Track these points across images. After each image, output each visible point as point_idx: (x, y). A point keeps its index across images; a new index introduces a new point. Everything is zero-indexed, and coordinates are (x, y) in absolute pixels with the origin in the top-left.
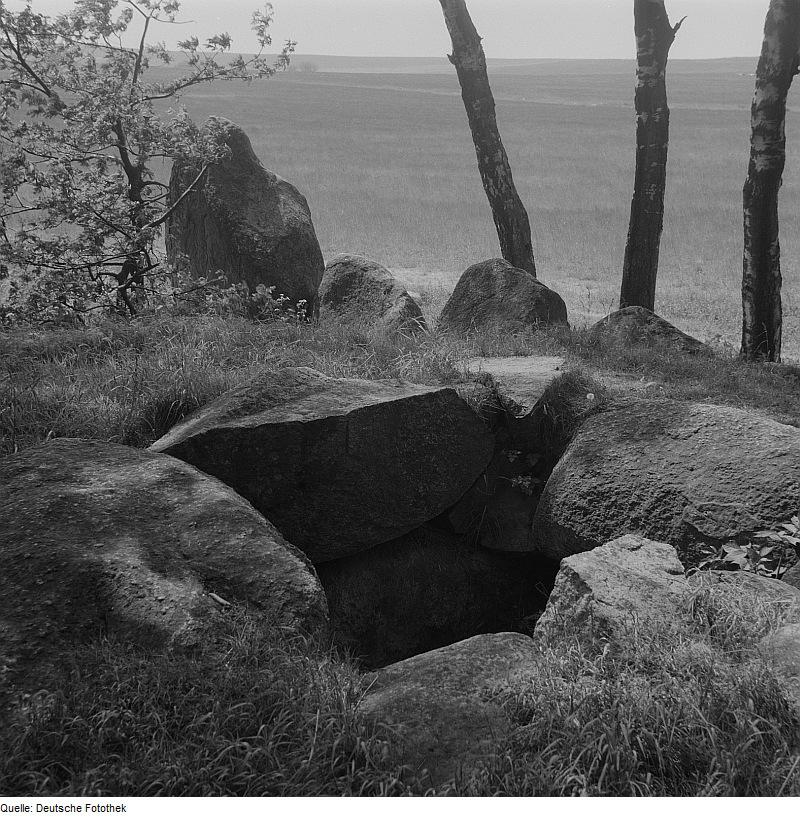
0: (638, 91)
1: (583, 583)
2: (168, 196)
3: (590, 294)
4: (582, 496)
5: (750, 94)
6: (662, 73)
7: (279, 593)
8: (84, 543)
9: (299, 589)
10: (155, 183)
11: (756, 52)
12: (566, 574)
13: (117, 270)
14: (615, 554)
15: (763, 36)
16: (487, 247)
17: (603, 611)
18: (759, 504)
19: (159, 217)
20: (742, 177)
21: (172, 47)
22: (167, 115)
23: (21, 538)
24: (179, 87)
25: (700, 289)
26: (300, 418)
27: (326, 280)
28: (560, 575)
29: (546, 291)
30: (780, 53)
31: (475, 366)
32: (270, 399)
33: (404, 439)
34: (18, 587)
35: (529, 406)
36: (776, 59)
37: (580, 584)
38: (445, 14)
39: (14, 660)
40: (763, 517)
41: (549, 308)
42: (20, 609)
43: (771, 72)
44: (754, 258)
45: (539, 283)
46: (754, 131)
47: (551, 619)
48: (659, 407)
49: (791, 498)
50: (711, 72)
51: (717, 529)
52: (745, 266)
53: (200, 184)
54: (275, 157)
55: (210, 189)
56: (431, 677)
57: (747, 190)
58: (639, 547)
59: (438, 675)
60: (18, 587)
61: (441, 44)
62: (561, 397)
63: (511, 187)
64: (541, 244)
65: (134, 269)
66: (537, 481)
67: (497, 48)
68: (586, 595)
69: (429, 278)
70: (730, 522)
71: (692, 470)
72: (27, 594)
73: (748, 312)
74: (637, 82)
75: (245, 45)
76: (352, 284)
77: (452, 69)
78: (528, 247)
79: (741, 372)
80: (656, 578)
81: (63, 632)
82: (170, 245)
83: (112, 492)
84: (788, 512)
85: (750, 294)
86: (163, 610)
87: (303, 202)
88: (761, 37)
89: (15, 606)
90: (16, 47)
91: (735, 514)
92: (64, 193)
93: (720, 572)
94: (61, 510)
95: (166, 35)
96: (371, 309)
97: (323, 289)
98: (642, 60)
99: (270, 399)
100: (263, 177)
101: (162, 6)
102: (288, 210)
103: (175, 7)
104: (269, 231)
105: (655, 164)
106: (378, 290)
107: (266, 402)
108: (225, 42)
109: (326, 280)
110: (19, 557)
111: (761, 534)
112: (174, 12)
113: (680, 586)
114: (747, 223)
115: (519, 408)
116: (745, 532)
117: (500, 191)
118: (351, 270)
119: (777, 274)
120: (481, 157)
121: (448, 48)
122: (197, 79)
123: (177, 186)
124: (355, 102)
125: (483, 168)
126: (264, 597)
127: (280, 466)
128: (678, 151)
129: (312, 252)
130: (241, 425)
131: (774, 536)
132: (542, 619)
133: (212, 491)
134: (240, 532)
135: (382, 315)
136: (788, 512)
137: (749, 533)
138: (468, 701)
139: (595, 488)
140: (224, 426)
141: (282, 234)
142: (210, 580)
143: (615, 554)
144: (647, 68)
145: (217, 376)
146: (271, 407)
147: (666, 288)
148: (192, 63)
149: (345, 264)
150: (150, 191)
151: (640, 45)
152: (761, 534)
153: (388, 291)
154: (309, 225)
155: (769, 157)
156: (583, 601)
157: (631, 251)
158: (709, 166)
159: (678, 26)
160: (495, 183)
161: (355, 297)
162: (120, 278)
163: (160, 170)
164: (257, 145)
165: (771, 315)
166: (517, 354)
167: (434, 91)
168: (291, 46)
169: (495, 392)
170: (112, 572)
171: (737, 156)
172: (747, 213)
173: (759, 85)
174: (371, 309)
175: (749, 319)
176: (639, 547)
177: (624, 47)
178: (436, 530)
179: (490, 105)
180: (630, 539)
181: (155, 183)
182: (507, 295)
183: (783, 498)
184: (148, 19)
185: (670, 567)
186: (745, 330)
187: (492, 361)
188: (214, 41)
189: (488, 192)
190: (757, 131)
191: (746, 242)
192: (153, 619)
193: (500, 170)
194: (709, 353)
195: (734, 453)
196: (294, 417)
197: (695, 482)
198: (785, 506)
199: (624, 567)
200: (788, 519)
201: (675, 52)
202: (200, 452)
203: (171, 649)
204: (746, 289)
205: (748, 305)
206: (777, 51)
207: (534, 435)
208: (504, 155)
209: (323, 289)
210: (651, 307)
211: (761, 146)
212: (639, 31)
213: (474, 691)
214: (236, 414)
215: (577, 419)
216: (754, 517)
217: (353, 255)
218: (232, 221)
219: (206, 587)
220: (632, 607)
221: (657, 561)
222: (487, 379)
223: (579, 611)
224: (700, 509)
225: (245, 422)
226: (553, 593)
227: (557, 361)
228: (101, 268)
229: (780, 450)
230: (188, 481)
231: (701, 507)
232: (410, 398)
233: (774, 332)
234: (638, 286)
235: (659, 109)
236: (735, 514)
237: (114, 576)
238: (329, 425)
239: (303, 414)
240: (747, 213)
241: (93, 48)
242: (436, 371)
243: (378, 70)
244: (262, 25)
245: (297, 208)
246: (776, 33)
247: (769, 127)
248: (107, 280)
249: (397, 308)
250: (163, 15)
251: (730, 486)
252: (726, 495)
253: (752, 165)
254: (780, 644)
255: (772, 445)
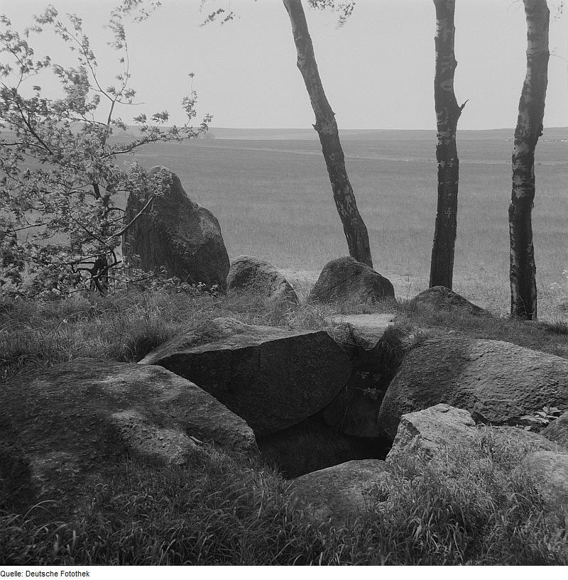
0: (438, 147)
1: (415, 428)
2: (124, 218)
3: (408, 277)
4: (409, 399)
5: (511, 149)
6: (453, 136)
7: (232, 437)
8: (111, 409)
9: (243, 434)
10: (117, 209)
11: (513, 124)
12: (404, 424)
13: (91, 266)
14: (433, 414)
15: (518, 112)
16: (340, 250)
17: (426, 444)
18: (522, 400)
19: (120, 231)
20: (509, 201)
21: (129, 122)
22: (125, 165)
23: (73, 406)
24: (135, 146)
25: (482, 277)
26: (230, 347)
27: (232, 273)
28: (401, 425)
29: (380, 278)
30: (530, 123)
31: (338, 320)
32: (209, 336)
33: (295, 363)
34: (75, 433)
35: (375, 341)
36: (527, 126)
37: (413, 429)
38: (311, 99)
39: (78, 471)
40: (525, 408)
41: (381, 290)
42: (77, 444)
43: (524, 134)
44: (517, 255)
45: (375, 272)
46: (514, 172)
47: (396, 453)
48: (457, 342)
49: (543, 395)
50: (486, 139)
51: (496, 416)
52: (511, 260)
53: (147, 210)
54: (198, 193)
55: (154, 213)
56: (326, 480)
57: (511, 210)
58: (447, 411)
59: (330, 479)
60: (75, 433)
61: (307, 118)
62: (391, 336)
63: (356, 210)
64: (375, 254)
65: (101, 266)
66: (380, 391)
67: (345, 123)
68: (417, 436)
69: (304, 273)
70: (504, 411)
71: (479, 380)
72: (80, 436)
73: (514, 291)
74: (437, 142)
75: (178, 119)
76: (249, 275)
77: (316, 136)
78: (368, 250)
79: (510, 325)
80: (458, 427)
81: (104, 457)
82: (125, 251)
83: (123, 382)
84: (541, 404)
85: (515, 278)
86: (163, 445)
87: (216, 222)
88: (517, 113)
89: (74, 443)
90: (27, 119)
91: (508, 406)
92: (64, 213)
93: (497, 427)
94: (94, 392)
95: (126, 114)
96: (262, 291)
97: (229, 279)
98: (440, 128)
99: (209, 336)
100: (189, 205)
101: (124, 93)
102: (206, 227)
103: (132, 93)
104: (193, 240)
105: (450, 194)
106: (267, 279)
107: (208, 338)
108: (165, 117)
109: (232, 273)
110: (73, 417)
111: (523, 418)
112: (131, 98)
113: (473, 432)
114: (512, 232)
115: (367, 343)
116: (514, 417)
117: (348, 213)
118: (248, 266)
119: (532, 265)
120: (335, 190)
121: (313, 120)
122: (146, 140)
123: (131, 211)
124: (252, 159)
125: (336, 197)
126: (222, 439)
127: (223, 373)
128: (466, 192)
129: (222, 254)
130: (193, 352)
131: (532, 419)
132: (390, 454)
133: (180, 382)
134: (205, 403)
135: (269, 295)
136: (541, 404)
137: (517, 418)
138: (349, 492)
139: (418, 393)
140: (181, 352)
141: (202, 242)
142: (190, 430)
143: (433, 414)
144: (443, 133)
145: (170, 326)
146: (210, 342)
147: (461, 282)
148: (143, 130)
149: (244, 262)
150: (113, 214)
151: (438, 118)
152: (523, 418)
153: (274, 280)
154: (220, 237)
155: (525, 189)
156: (415, 440)
157: (436, 252)
158: (486, 198)
159: (463, 106)
160: (345, 208)
161: (251, 284)
162: (93, 272)
163: (120, 200)
164: (185, 186)
165: (529, 292)
166: (364, 313)
167: (296, 152)
168: (209, 118)
169: (352, 334)
170: (131, 424)
171: (503, 193)
172: (512, 225)
173: (516, 143)
174: (262, 291)
175: (515, 294)
176: (447, 411)
177: (428, 121)
178: (320, 405)
179: (341, 157)
180: (441, 406)
181: (117, 209)
182: (353, 276)
183: (537, 395)
184: (114, 102)
185: (467, 422)
186: (513, 303)
187: (349, 317)
188: (158, 116)
189: (340, 213)
190: (516, 172)
191: (512, 244)
192: (157, 450)
193: (348, 199)
194: (488, 314)
195: (505, 369)
196: (225, 347)
197: (482, 387)
198: (539, 400)
199: (439, 421)
200: (541, 409)
201: (463, 124)
202: (176, 364)
203: (169, 466)
204: (512, 274)
205: (514, 286)
206: (528, 121)
207: (373, 364)
208: (351, 189)
209: (229, 279)
210: (449, 285)
211: (519, 182)
212: (438, 109)
213: (353, 487)
214: (189, 345)
215: (404, 351)
216: (520, 408)
217: (250, 256)
218: (167, 232)
219: (187, 433)
220: (445, 443)
221: (459, 418)
222: (349, 325)
223: (412, 446)
224: (485, 404)
225: (195, 350)
226: (397, 437)
227: (392, 316)
228: (80, 266)
229: (535, 366)
230: (168, 377)
231: (486, 402)
232: (298, 337)
233: (532, 303)
234: (442, 270)
235: (452, 159)
236: (508, 406)
237: (132, 426)
238: (249, 352)
239: (232, 345)
240: (512, 225)
241: (75, 122)
242: (311, 322)
243: (256, 138)
244: (189, 107)
245: (212, 225)
246: (526, 110)
247: (524, 169)
248: (83, 273)
249: (279, 291)
250: (124, 99)
251: (503, 389)
252: (501, 394)
253: (514, 194)
254: (532, 461)
255: (530, 363)
